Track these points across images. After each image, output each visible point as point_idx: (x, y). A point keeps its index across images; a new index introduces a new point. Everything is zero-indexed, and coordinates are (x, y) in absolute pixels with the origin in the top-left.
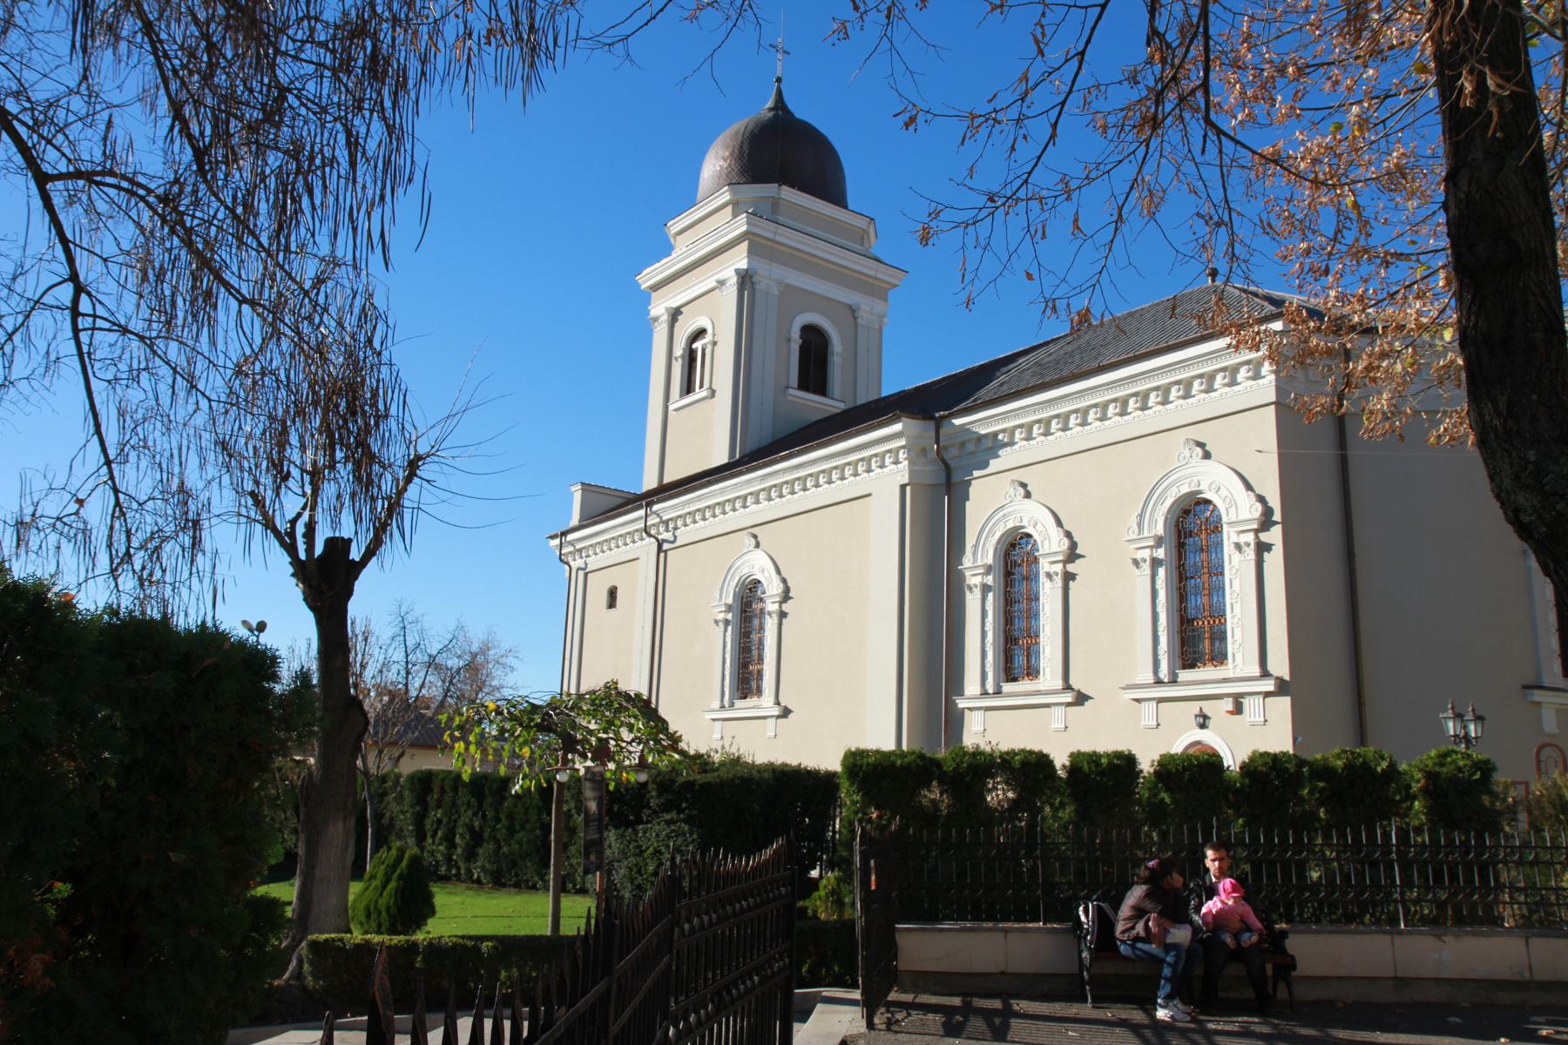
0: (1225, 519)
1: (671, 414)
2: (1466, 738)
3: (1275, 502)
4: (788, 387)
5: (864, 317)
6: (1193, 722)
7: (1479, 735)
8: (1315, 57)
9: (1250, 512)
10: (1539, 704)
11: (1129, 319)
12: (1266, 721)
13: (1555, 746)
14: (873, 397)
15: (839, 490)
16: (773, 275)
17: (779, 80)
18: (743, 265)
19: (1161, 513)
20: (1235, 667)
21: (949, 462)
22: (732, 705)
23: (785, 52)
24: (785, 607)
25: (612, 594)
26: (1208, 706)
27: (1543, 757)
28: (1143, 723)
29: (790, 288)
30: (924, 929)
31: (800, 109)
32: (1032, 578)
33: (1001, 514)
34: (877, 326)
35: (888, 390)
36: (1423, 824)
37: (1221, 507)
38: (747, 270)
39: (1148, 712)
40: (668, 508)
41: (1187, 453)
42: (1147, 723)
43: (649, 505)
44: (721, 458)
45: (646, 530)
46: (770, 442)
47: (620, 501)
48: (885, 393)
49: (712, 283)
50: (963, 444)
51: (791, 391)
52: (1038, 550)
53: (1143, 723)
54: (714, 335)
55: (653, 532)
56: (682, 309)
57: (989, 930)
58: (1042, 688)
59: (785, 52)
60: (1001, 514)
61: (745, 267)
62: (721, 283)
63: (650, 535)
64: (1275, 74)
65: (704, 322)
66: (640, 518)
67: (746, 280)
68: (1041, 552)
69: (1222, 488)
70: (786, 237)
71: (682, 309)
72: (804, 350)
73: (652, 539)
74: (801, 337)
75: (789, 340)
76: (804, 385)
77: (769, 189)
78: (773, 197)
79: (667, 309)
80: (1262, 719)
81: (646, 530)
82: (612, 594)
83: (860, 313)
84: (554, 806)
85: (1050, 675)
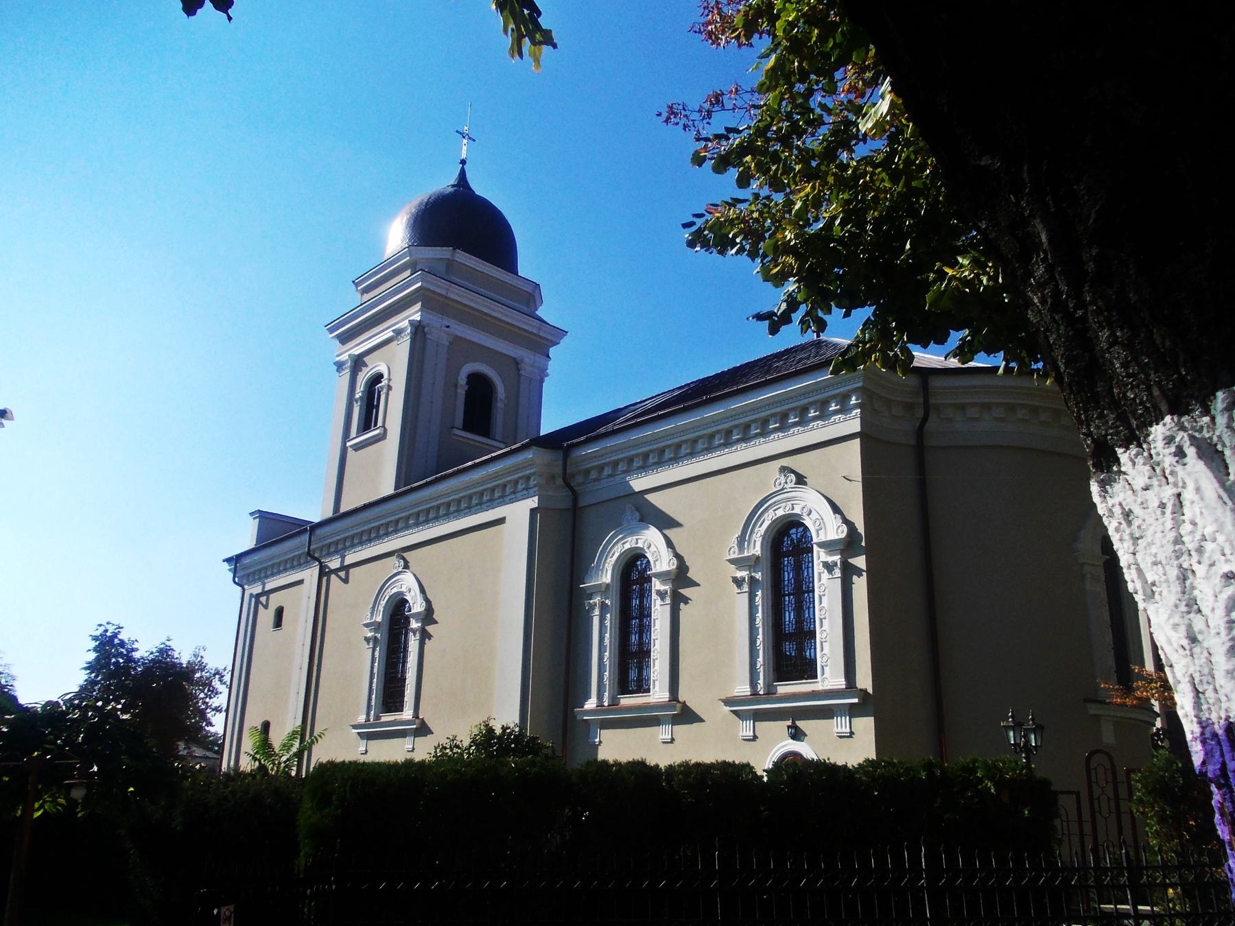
0: (815, 540)
2: (1027, 748)
3: (861, 528)
4: (453, 427)
5: (526, 370)
7: (1039, 744)
9: (837, 532)
10: (1097, 717)
12: (852, 733)
13: (1105, 753)
16: (445, 329)
17: (463, 162)
18: (417, 317)
19: (759, 535)
20: (823, 681)
21: (576, 488)
22: (377, 717)
23: (470, 138)
25: (279, 613)
27: (1093, 765)
28: (741, 734)
29: (457, 338)
31: (480, 187)
32: (644, 594)
34: (538, 378)
38: (420, 321)
39: (746, 728)
41: (783, 479)
42: (745, 734)
45: (310, 554)
49: (389, 334)
50: (587, 472)
51: (456, 431)
52: (650, 570)
54: (390, 380)
56: (366, 359)
59: (470, 138)
61: (419, 319)
62: (399, 333)
65: (383, 369)
67: (418, 330)
68: (654, 571)
69: (813, 512)
70: (456, 294)
71: (366, 359)
74: (467, 383)
75: (456, 386)
76: (467, 427)
77: (443, 252)
78: (448, 259)
79: (349, 355)
80: (848, 730)
81: (310, 554)
82: (279, 613)
83: (522, 366)
84: (928, 912)
85: (659, 693)
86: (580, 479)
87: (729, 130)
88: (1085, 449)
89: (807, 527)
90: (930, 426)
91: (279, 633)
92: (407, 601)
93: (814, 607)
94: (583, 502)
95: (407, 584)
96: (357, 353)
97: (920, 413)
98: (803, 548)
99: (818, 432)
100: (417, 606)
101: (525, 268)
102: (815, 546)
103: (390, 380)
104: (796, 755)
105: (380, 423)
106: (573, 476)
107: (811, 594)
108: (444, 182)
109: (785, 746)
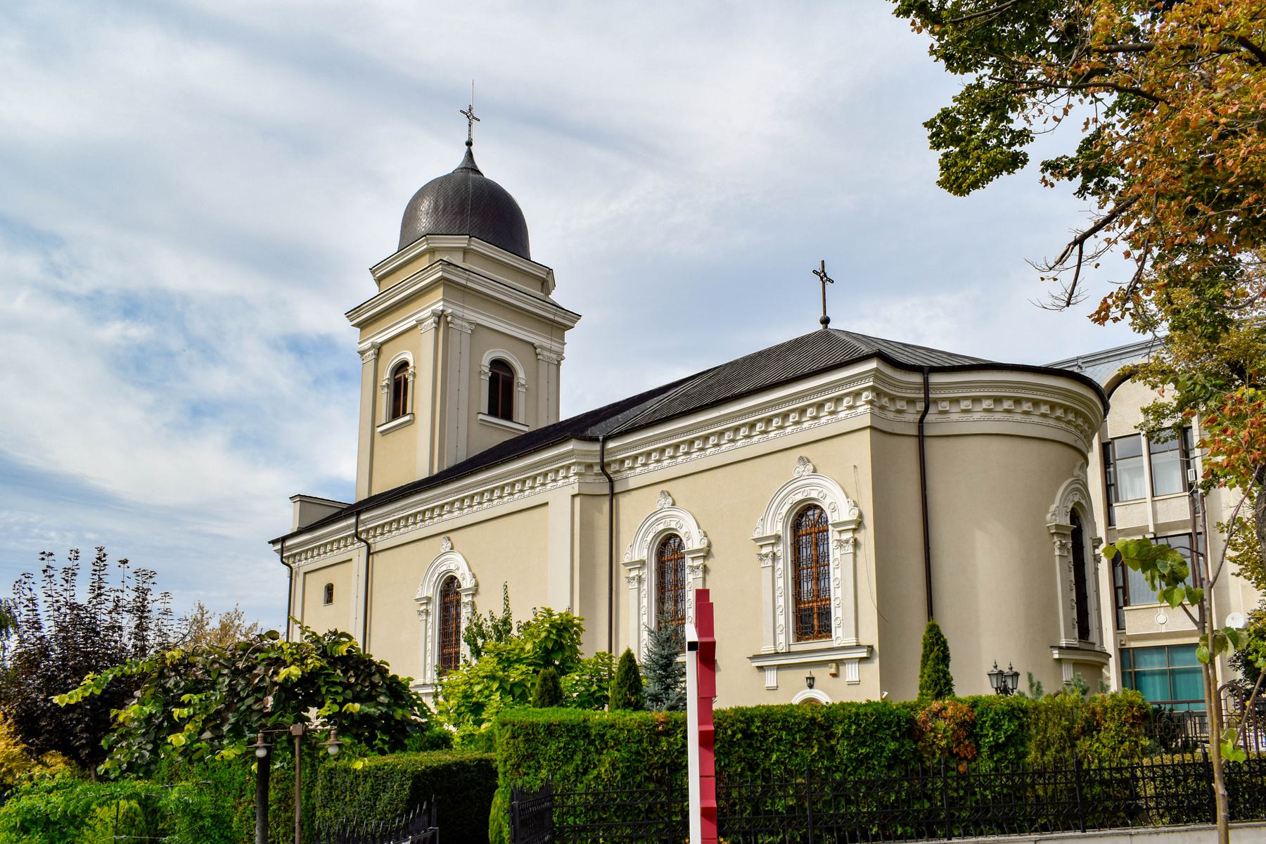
1: (377, 436)
6: (805, 684)
8: (1087, 124)
11: (759, 358)
14: (552, 422)
15: (519, 502)
18: (439, 307)
21: (612, 476)
24: (709, 563)
25: (329, 589)
26: (815, 672)
30: (1071, 837)
32: (458, 603)
33: (655, 518)
35: (566, 413)
36: (923, 762)
37: (828, 512)
40: (370, 518)
43: (358, 514)
44: (422, 473)
45: (357, 535)
46: (464, 459)
47: (331, 512)
48: (562, 419)
49: (411, 322)
53: (847, 680)
55: (363, 536)
57: (1183, 831)
58: (835, 644)
60: (655, 518)
63: (360, 540)
64: (1098, 123)
65: (409, 357)
66: (348, 527)
67: (440, 317)
72: (493, 381)
73: (363, 544)
76: (493, 411)
81: (357, 535)
82: (329, 589)
86: (615, 467)
87: (1039, 687)
88: (1047, 511)
89: (822, 509)
90: (928, 418)
91: (330, 607)
92: (456, 578)
93: (829, 578)
94: (617, 490)
95: (457, 564)
96: (380, 341)
97: (920, 406)
98: (821, 528)
99: (826, 425)
100: (466, 583)
101: (539, 250)
102: (830, 527)
103: (415, 367)
104: (497, 775)
105: (409, 411)
106: (609, 464)
107: (826, 568)
108: (448, 162)
109: (804, 694)
